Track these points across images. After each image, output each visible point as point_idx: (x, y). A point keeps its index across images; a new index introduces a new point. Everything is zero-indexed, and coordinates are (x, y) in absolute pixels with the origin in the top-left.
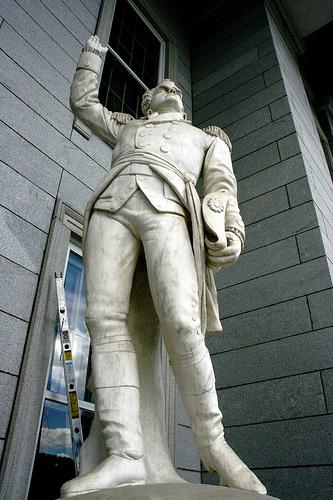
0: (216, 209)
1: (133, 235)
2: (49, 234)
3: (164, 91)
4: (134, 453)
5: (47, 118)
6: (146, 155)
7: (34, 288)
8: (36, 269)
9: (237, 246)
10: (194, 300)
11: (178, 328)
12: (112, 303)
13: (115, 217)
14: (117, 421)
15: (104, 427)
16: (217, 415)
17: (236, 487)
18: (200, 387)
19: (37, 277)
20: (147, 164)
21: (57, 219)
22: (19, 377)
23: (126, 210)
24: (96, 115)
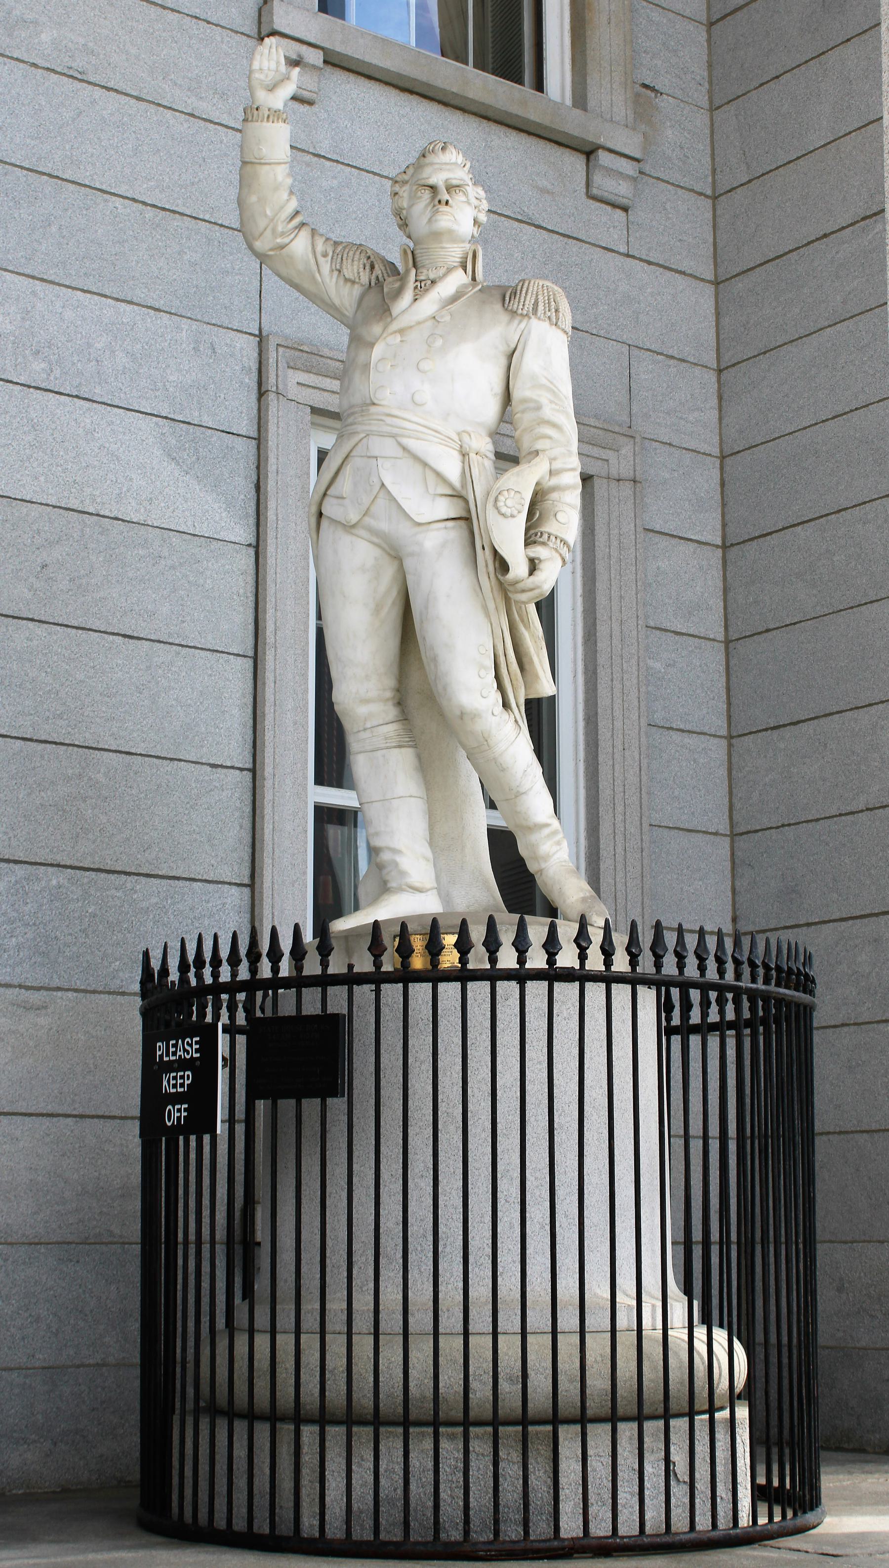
1: (389, 554)
2: (260, 440)
4: (417, 885)
5: (192, 103)
7: (251, 579)
8: (243, 533)
11: (458, 713)
12: (367, 678)
13: (355, 531)
14: (392, 845)
18: (511, 790)
19: (252, 551)
20: (394, 436)
21: (272, 396)
22: (253, 771)
24: (301, 267)
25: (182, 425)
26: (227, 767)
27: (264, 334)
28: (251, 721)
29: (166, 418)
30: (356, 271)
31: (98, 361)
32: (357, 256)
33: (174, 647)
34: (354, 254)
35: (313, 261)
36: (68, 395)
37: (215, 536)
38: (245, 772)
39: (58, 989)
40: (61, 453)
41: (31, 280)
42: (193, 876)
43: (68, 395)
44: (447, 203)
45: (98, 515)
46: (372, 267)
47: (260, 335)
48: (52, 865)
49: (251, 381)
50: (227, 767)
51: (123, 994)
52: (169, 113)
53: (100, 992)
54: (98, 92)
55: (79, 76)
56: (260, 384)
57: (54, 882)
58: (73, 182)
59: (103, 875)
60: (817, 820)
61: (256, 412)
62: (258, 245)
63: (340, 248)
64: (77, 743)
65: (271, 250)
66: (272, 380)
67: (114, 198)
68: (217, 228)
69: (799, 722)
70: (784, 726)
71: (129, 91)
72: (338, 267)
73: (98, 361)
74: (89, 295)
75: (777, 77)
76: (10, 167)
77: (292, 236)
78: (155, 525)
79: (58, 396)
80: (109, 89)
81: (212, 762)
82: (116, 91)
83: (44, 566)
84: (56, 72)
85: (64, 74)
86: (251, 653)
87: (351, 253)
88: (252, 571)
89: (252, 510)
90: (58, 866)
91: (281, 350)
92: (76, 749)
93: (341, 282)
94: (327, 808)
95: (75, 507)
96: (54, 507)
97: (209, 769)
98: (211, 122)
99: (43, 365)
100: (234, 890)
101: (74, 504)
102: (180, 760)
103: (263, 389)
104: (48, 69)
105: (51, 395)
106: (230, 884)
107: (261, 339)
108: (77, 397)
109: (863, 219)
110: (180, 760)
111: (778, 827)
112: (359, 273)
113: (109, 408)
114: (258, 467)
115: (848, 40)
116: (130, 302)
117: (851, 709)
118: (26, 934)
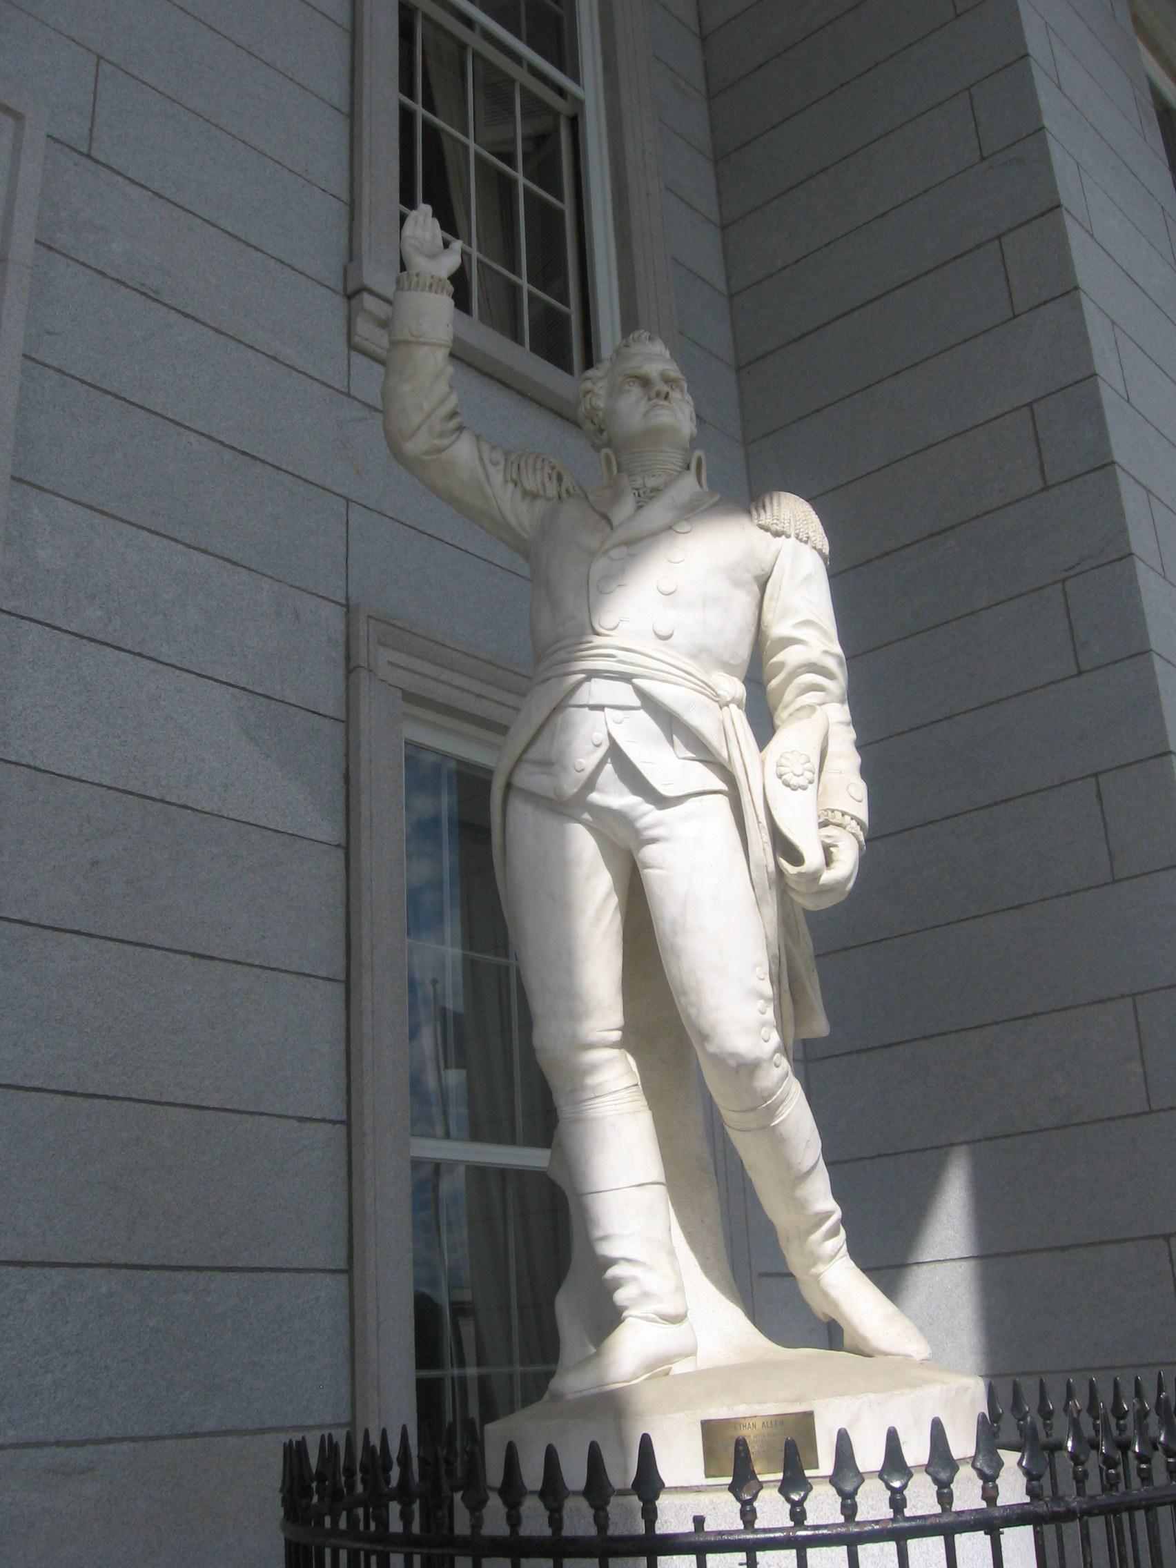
0: (795, 781)
3: (636, 391)
6: (621, 655)
8: (330, 831)
9: (846, 864)
10: (762, 997)
15: (815, 1264)
16: (828, 1215)
17: (886, 1354)
20: (626, 678)
22: (348, 1123)
23: (595, 797)
25: (262, 699)
26: (317, 1120)
27: (351, 604)
28: (344, 1061)
29: (244, 689)
30: (539, 481)
31: (165, 615)
32: (539, 465)
33: (254, 970)
34: (535, 462)
35: (480, 469)
36: (129, 652)
37: (301, 833)
38: (338, 1126)
39: (110, 1440)
40: (120, 722)
41: (89, 511)
42: (280, 1265)
43: (129, 652)
44: (666, 397)
45: (162, 801)
46: (560, 478)
47: (347, 606)
48: (100, 1265)
49: (338, 654)
50: (317, 1120)
51: (195, 1435)
52: (250, 353)
53: (164, 1438)
54: (173, 316)
55: (153, 295)
56: (348, 658)
57: (104, 1289)
58: (142, 407)
59: (167, 1274)
60: (924, 1150)
61: (343, 690)
62: (410, 447)
63: (513, 457)
64: (134, 1096)
65: (427, 453)
66: (363, 653)
67: (188, 433)
68: (301, 482)
69: (890, 1045)
70: (874, 1049)
71: (208, 322)
72: (515, 476)
73: (165, 615)
74: (157, 538)
75: (818, 411)
76: (69, 379)
77: (453, 437)
78: (232, 816)
79: (117, 652)
80: (187, 315)
81: (299, 1114)
82: (193, 318)
83: (95, 863)
84: (127, 286)
85: (136, 290)
86: (342, 977)
87: (530, 461)
88: (342, 877)
89: (340, 804)
90: (110, 1265)
91: (372, 622)
92: (132, 1104)
93: (519, 495)
94: (516, 1171)
95: (135, 790)
96: (109, 788)
97: (295, 1123)
98: (295, 369)
99: (99, 613)
100: (328, 1279)
101: (133, 785)
102: (261, 1114)
103: (352, 665)
104: (118, 281)
105: (109, 650)
106: (324, 1271)
107: (348, 608)
108: (140, 655)
109: (931, 536)
110: (261, 1114)
111: (872, 1158)
112: (543, 484)
113: (178, 672)
114: (347, 755)
115: (897, 373)
116: (204, 551)
117: (957, 1031)
118: (65, 1366)
